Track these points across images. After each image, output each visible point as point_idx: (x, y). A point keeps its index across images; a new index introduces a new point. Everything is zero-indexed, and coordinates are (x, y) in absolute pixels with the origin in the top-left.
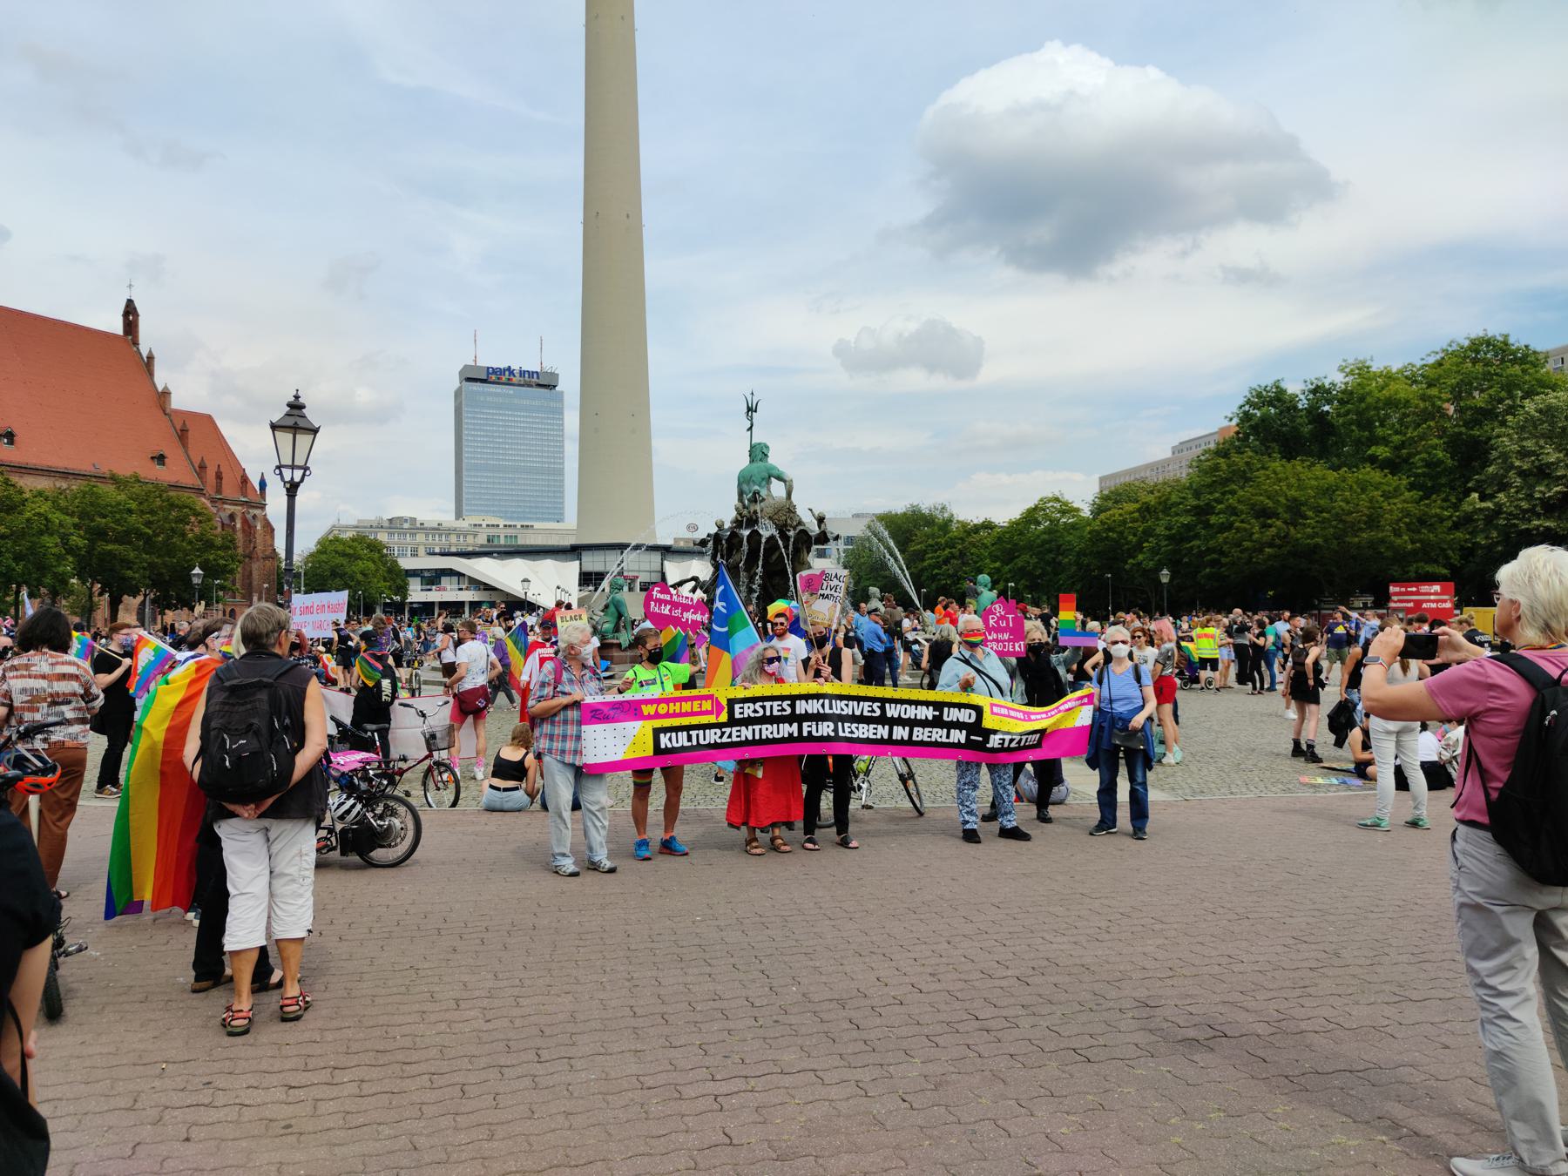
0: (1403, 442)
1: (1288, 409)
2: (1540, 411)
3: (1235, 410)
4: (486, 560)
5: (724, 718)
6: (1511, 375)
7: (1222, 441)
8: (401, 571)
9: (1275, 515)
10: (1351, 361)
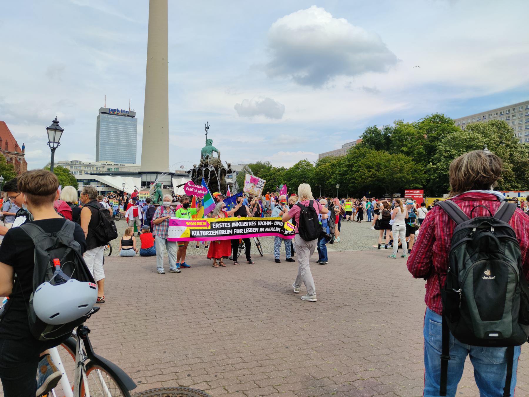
0: (411, 146)
1: (378, 135)
2: (452, 138)
3: (362, 134)
4: (107, 177)
5: (209, 228)
6: (444, 127)
7: (357, 144)
8: (75, 180)
9: (373, 168)
10: (397, 120)
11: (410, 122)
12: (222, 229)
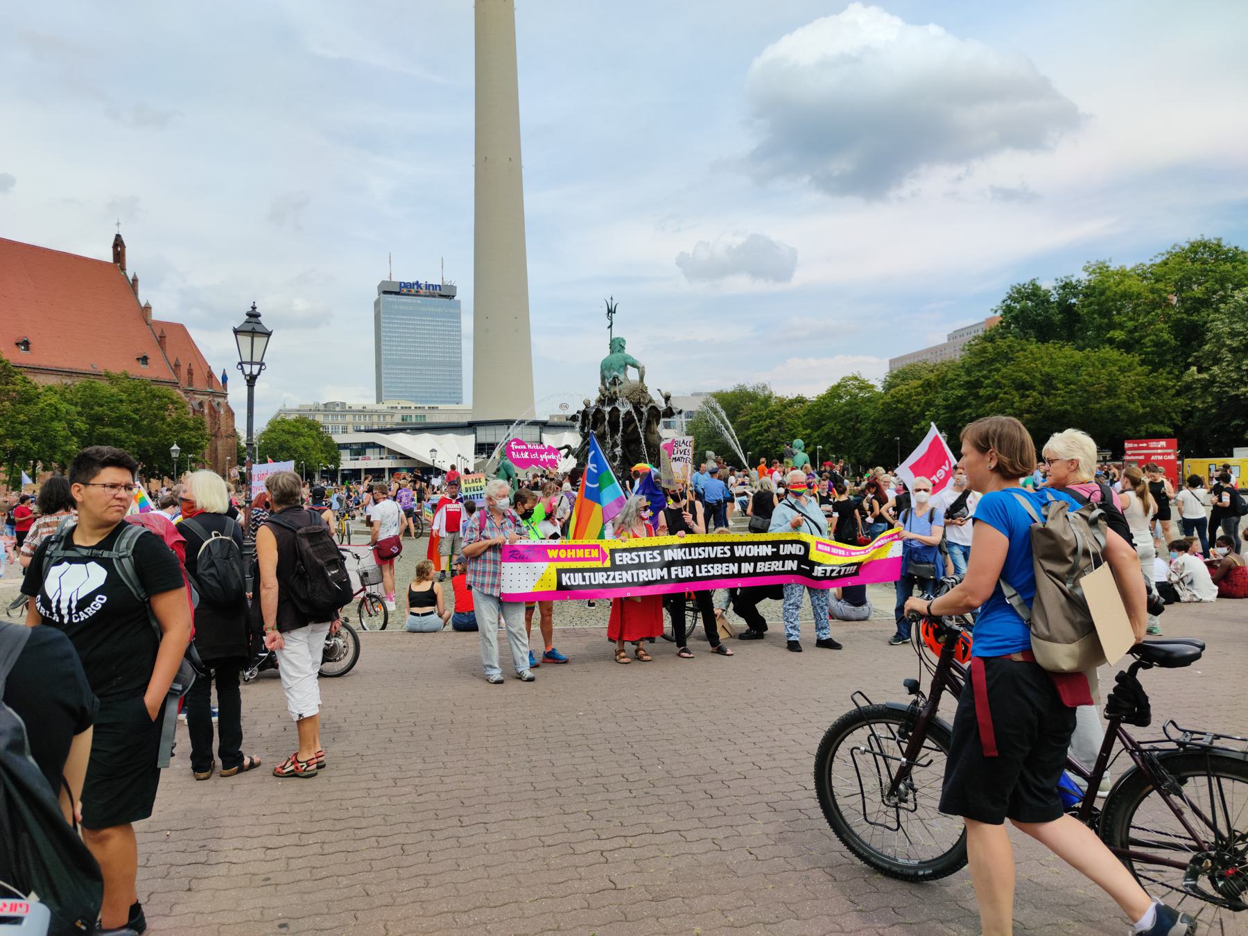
0: (1136, 327)
3: (999, 304)
4: (401, 435)
5: (608, 564)
6: (1224, 271)
7: (988, 329)
9: (1032, 387)
10: (1093, 262)
11: (1129, 266)
12: (640, 566)
